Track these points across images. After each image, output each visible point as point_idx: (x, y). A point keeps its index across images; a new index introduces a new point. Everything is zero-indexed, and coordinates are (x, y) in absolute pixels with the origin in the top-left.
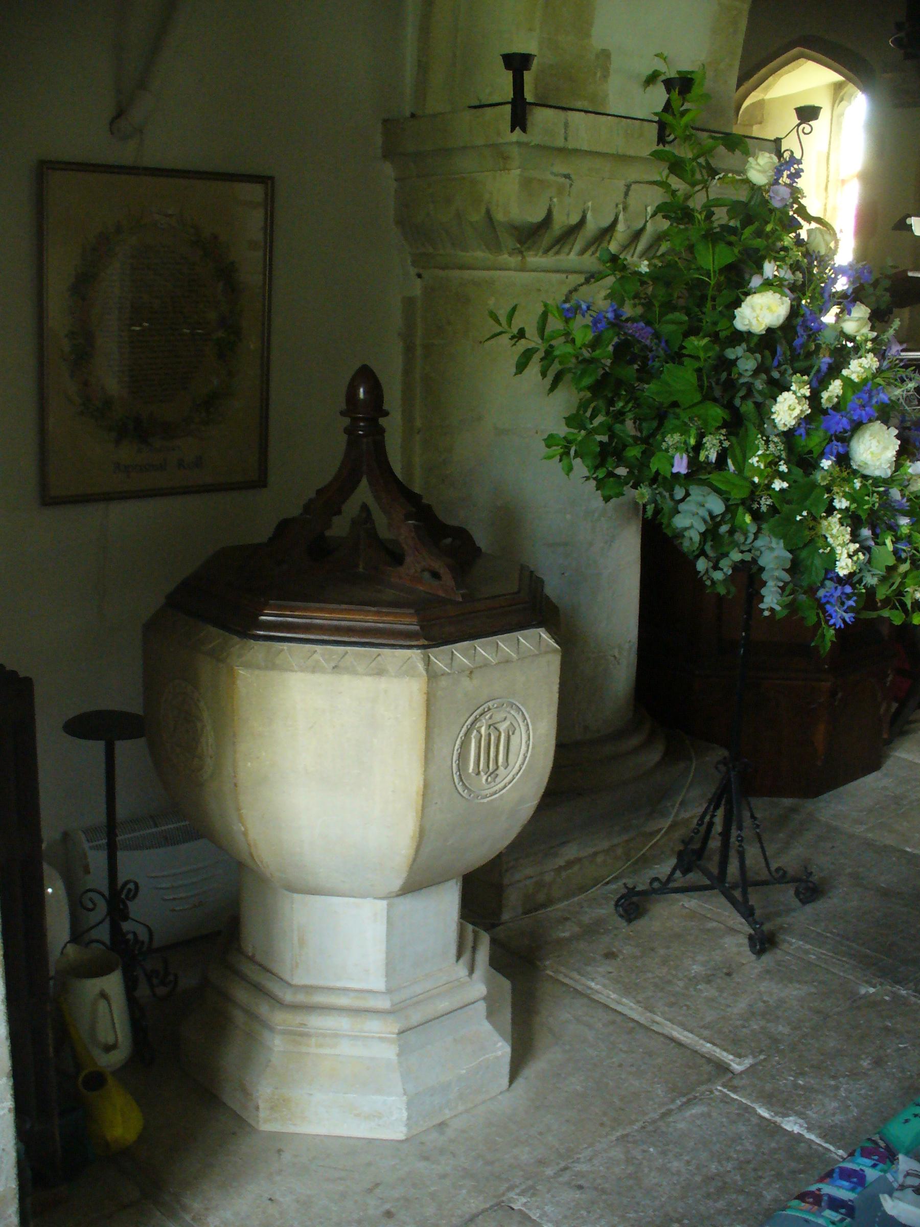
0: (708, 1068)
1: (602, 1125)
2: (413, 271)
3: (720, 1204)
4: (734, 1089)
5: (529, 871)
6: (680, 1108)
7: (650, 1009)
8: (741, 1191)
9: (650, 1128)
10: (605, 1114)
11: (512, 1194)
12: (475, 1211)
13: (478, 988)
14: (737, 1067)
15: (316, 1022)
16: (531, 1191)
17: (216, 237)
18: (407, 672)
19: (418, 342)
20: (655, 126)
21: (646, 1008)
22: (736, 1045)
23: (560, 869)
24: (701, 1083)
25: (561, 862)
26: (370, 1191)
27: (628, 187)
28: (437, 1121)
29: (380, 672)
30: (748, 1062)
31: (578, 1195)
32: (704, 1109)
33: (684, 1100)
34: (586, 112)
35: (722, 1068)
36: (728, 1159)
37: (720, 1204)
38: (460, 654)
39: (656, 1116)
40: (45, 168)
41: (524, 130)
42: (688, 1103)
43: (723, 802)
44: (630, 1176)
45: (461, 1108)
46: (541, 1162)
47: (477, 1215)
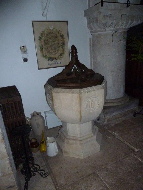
0: (131, 151)
1: (113, 159)
2: (90, 34)
3: (130, 177)
4: (135, 155)
5: (108, 116)
6: (126, 158)
7: (123, 139)
8: (134, 175)
9: (121, 161)
10: (114, 157)
11: (96, 171)
12: (90, 173)
13: (95, 137)
14: (136, 150)
15: (70, 141)
16: (99, 171)
17: (60, 31)
18: (77, 93)
19: (92, 44)
20: (126, 4)
21: (123, 139)
22: (137, 147)
23: (113, 116)
24: (130, 153)
25: (113, 115)
26: (76, 168)
27: (122, 15)
28: (88, 156)
29: (73, 93)
30: (138, 150)
31: (107, 172)
32: (130, 158)
33: (127, 156)
34: (114, 3)
35: (134, 151)
36: (133, 168)
37: (130, 177)
38: (82, 90)
39: (122, 158)
40: (33, 22)
41: (103, 6)
42: (128, 157)
43: (111, 132)
44: (116, 170)
45: (92, 154)
46: (102, 165)
47: (90, 174)
